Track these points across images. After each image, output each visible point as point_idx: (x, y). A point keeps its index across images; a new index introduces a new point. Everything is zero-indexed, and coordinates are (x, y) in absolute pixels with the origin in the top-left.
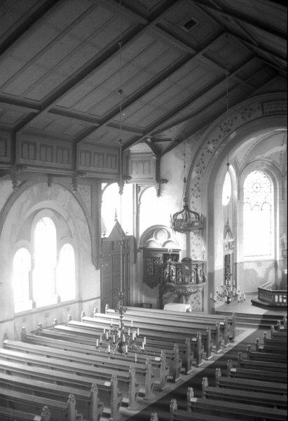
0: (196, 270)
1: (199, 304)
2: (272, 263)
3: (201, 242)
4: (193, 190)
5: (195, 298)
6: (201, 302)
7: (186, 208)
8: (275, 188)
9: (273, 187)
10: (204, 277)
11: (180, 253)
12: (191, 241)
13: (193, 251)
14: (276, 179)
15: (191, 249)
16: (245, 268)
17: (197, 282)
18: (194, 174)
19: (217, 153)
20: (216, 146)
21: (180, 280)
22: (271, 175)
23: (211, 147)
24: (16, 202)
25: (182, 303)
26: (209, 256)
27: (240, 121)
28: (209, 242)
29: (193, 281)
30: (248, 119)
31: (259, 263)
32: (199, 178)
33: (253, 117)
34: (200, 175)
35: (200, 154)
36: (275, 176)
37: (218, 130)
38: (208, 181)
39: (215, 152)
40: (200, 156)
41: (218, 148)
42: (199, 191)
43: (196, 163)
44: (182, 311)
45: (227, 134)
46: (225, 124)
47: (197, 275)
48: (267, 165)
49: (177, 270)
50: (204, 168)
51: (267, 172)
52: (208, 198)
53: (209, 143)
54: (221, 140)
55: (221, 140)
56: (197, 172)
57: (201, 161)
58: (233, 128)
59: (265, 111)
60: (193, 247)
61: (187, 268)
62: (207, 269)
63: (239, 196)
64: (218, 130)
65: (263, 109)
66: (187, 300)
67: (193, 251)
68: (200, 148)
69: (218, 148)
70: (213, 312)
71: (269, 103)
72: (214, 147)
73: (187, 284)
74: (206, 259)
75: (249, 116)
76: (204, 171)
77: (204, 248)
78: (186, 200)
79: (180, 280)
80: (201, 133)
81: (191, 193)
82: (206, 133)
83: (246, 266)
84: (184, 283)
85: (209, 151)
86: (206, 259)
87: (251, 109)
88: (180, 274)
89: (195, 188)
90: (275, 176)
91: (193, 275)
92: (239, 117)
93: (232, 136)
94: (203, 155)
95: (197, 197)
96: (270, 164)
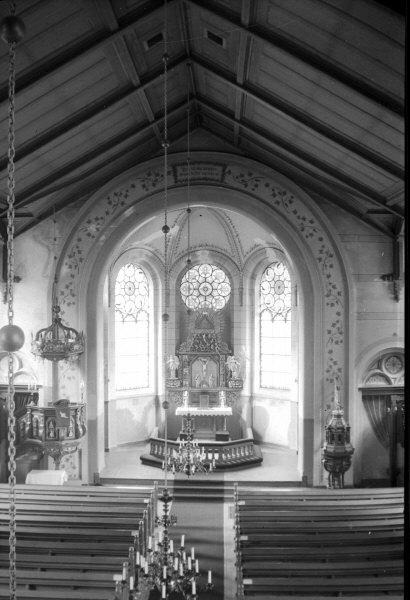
0: (75, 417)
1: (74, 468)
2: (152, 399)
3: (77, 373)
4: (62, 293)
5: (68, 460)
6: (77, 466)
7: (57, 321)
8: (156, 289)
9: (151, 287)
10: (83, 427)
11: (41, 393)
12: (61, 372)
13: (64, 387)
14: (158, 276)
15: (60, 385)
16: (117, 408)
17: (77, 436)
18: (65, 270)
19: (103, 238)
20: (101, 227)
21: (52, 434)
22: (151, 270)
23: (92, 228)
24: (297, 393)
25: (47, 468)
26: (88, 395)
27: (139, 192)
28: (88, 370)
29: (71, 434)
30: (152, 189)
31: (135, 400)
32: (73, 276)
33: (159, 186)
34: (75, 272)
35: (75, 238)
36: (157, 272)
37: (105, 202)
38: (88, 281)
39: (101, 236)
40: (74, 242)
41: (103, 230)
42: (73, 296)
43: (69, 252)
44: (56, 483)
45: (121, 208)
46: (116, 194)
47: (77, 425)
48: (147, 255)
49: (46, 418)
50: (81, 260)
51: (145, 266)
52: (88, 306)
53: (89, 222)
54: (109, 218)
55: (109, 218)
56: (70, 267)
57: (76, 250)
58: (128, 201)
59: (179, 178)
60: (62, 382)
61: (63, 415)
62: (87, 415)
63: (109, 301)
64: (105, 202)
65: (175, 176)
66: (58, 464)
67: (64, 387)
68: (75, 229)
69: (103, 230)
70: (97, 481)
71: (196, 166)
72: (98, 229)
73: (63, 440)
74: (85, 401)
75: (154, 185)
76: (81, 265)
77: (83, 384)
78: (56, 309)
79: (52, 434)
80: (77, 207)
81: (60, 298)
82: (86, 206)
83: (121, 405)
84: (57, 438)
85: (89, 235)
86: (85, 401)
87: (157, 175)
88: (51, 425)
89: (67, 292)
90: (157, 272)
91: (71, 425)
92: (139, 185)
93: (129, 212)
94: (79, 240)
95: (69, 304)
96: (150, 254)
